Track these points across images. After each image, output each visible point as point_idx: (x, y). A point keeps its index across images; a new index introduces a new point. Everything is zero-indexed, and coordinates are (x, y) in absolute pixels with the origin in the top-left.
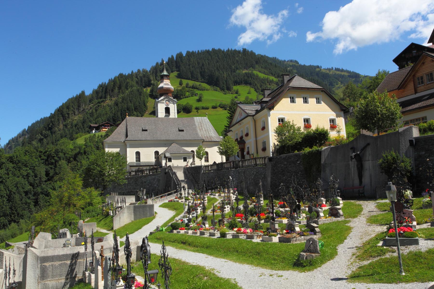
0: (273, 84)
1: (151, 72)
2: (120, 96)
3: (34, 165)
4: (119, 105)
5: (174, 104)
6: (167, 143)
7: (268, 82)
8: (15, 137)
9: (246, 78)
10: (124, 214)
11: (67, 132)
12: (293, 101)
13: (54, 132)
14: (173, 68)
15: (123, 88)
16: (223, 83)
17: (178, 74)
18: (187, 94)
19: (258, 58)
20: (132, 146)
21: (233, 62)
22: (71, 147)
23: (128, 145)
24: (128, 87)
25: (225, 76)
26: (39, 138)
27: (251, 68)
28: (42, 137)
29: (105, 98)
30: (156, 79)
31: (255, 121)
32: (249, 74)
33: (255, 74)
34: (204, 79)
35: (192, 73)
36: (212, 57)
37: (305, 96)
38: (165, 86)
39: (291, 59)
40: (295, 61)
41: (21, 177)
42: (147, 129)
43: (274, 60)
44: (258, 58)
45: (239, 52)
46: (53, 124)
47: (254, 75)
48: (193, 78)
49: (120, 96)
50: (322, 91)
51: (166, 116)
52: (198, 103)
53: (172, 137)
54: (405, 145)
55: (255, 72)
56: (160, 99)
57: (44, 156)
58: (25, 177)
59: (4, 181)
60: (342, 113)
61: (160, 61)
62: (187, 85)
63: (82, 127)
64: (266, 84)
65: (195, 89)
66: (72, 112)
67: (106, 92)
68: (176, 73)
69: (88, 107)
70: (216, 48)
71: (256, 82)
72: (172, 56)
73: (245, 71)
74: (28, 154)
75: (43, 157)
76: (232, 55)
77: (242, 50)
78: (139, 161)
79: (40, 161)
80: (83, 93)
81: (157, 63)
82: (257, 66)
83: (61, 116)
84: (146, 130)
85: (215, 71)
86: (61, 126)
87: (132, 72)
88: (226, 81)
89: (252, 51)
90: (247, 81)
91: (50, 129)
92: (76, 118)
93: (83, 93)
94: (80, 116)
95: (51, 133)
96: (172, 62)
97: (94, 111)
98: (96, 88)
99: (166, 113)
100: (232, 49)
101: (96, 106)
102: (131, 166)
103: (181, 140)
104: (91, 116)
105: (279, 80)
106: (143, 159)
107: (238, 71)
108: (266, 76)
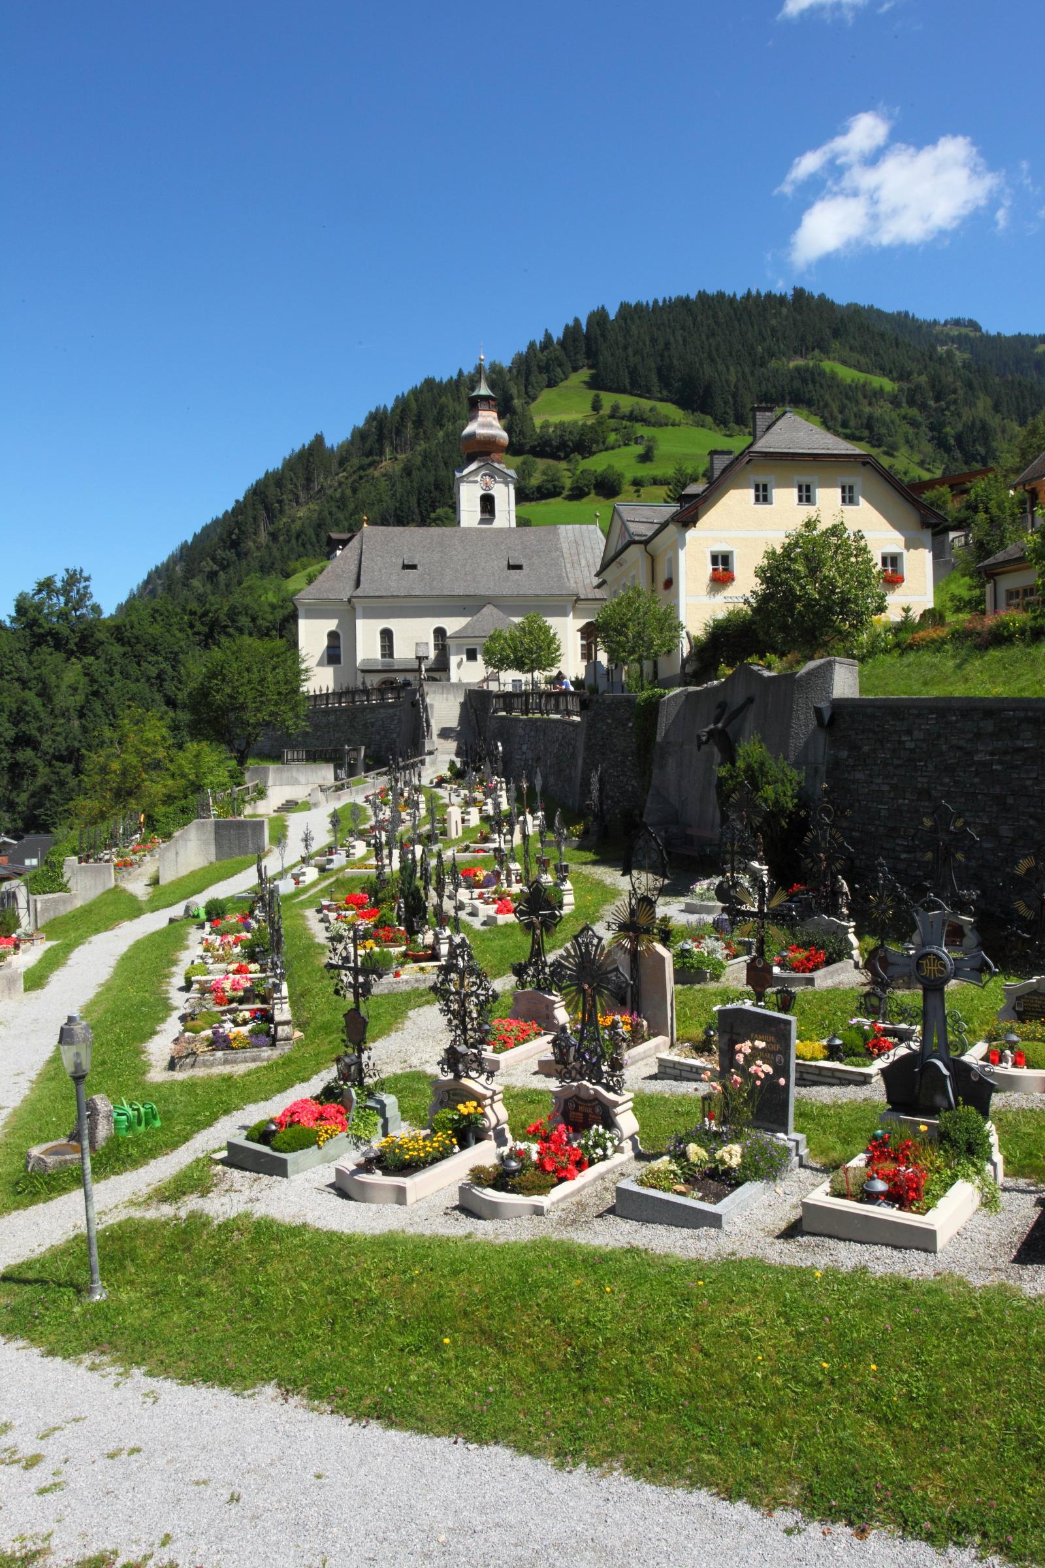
0: (881, 403)
1: (514, 371)
2: (419, 448)
3: (176, 649)
4: (415, 473)
5: (507, 485)
6: (466, 605)
7: (865, 397)
8: (163, 564)
9: (797, 384)
10: (189, 844)
11: (276, 553)
12: (763, 496)
13: (246, 554)
14: (578, 356)
15: (428, 424)
16: (726, 403)
17: (593, 377)
18: (612, 437)
19: (842, 320)
20: (371, 614)
21: (760, 333)
22: (271, 597)
23: (359, 611)
24: (445, 420)
25: (733, 379)
26: (208, 569)
27: (817, 352)
28: (216, 568)
29: (381, 453)
30: (526, 393)
31: (653, 559)
32: (807, 369)
33: (828, 370)
34: (670, 391)
35: (633, 373)
36: (695, 319)
37: (805, 480)
38: (482, 431)
39: (956, 316)
40: (970, 321)
41: (143, 680)
42: (415, 562)
43: (903, 321)
44: (842, 320)
45: (782, 300)
46: (242, 532)
47: (822, 373)
48: (637, 387)
49: (419, 448)
50: (865, 462)
51: (482, 521)
52: (641, 465)
53: (484, 588)
54: (803, 726)
55: (828, 365)
56: (466, 472)
57: (202, 623)
58: (154, 681)
59: (102, 691)
60: (927, 535)
61: (539, 338)
62: (615, 408)
63: (314, 540)
64: (857, 403)
65: (637, 421)
66: (291, 497)
67: (381, 438)
68: (585, 374)
69: (331, 482)
70: (712, 290)
71: (827, 397)
72: (577, 320)
73: (797, 362)
74: (159, 619)
75: (199, 627)
76: (757, 310)
77: (790, 292)
78: (391, 655)
79: (192, 639)
80: (319, 439)
81: (532, 345)
82: (835, 345)
83: (260, 507)
84: (414, 567)
85: (701, 364)
86: (263, 537)
87: (460, 373)
88: (734, 396)
89: (822, 297)
90: (800, 394)
91: (235, 545)
92: (300, 514)
93: (319, 439)
94: (312, 506)
95: (238, 555)
96: (575, 340)
97: (348, 492)
98: (361, 423)
99: (483, 511)
100: (758, 293)
101: (355, 477)
102: (363, 671)
103: (512, 596)
104: (339, 507)
105: (901, 390)
106: (404, 651)
107: (773, 364)
108: (861, 377)
